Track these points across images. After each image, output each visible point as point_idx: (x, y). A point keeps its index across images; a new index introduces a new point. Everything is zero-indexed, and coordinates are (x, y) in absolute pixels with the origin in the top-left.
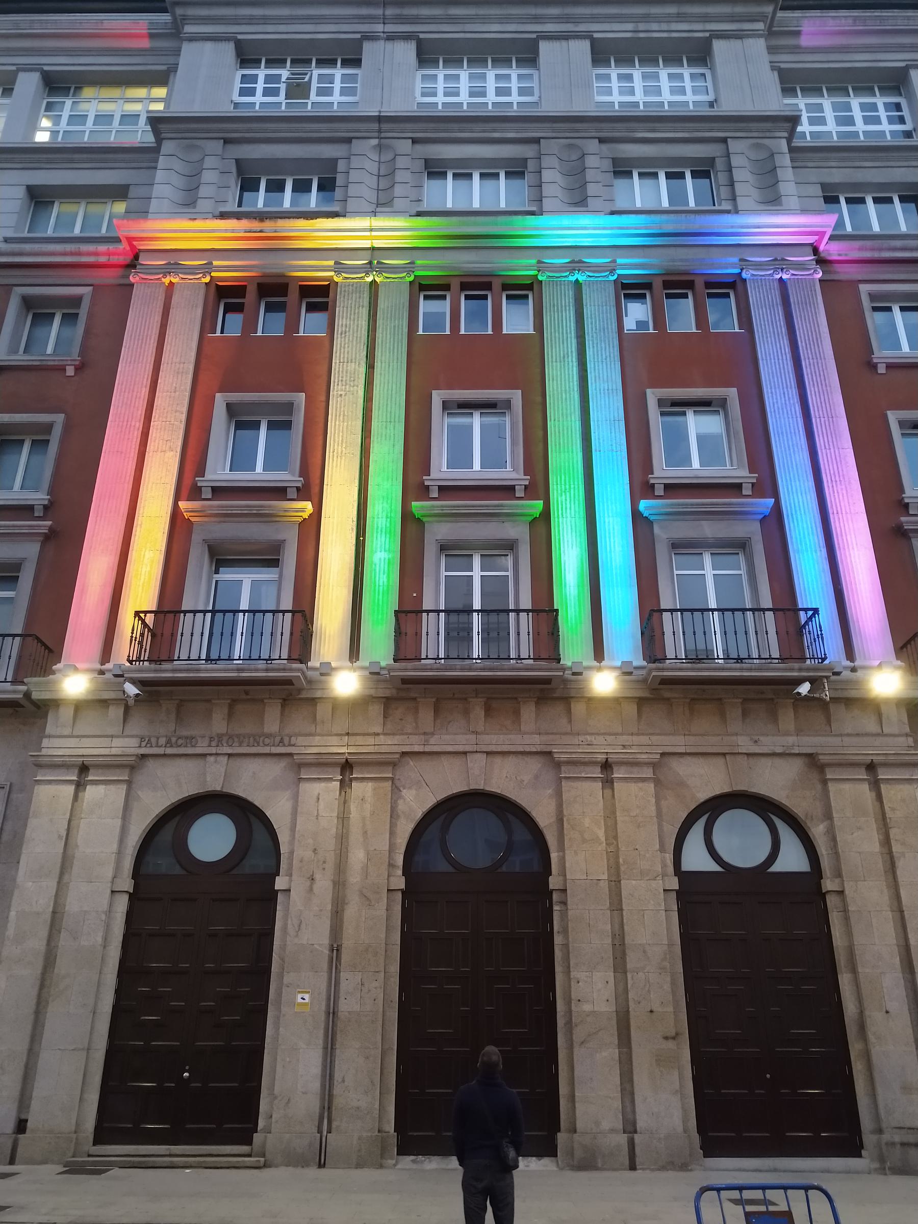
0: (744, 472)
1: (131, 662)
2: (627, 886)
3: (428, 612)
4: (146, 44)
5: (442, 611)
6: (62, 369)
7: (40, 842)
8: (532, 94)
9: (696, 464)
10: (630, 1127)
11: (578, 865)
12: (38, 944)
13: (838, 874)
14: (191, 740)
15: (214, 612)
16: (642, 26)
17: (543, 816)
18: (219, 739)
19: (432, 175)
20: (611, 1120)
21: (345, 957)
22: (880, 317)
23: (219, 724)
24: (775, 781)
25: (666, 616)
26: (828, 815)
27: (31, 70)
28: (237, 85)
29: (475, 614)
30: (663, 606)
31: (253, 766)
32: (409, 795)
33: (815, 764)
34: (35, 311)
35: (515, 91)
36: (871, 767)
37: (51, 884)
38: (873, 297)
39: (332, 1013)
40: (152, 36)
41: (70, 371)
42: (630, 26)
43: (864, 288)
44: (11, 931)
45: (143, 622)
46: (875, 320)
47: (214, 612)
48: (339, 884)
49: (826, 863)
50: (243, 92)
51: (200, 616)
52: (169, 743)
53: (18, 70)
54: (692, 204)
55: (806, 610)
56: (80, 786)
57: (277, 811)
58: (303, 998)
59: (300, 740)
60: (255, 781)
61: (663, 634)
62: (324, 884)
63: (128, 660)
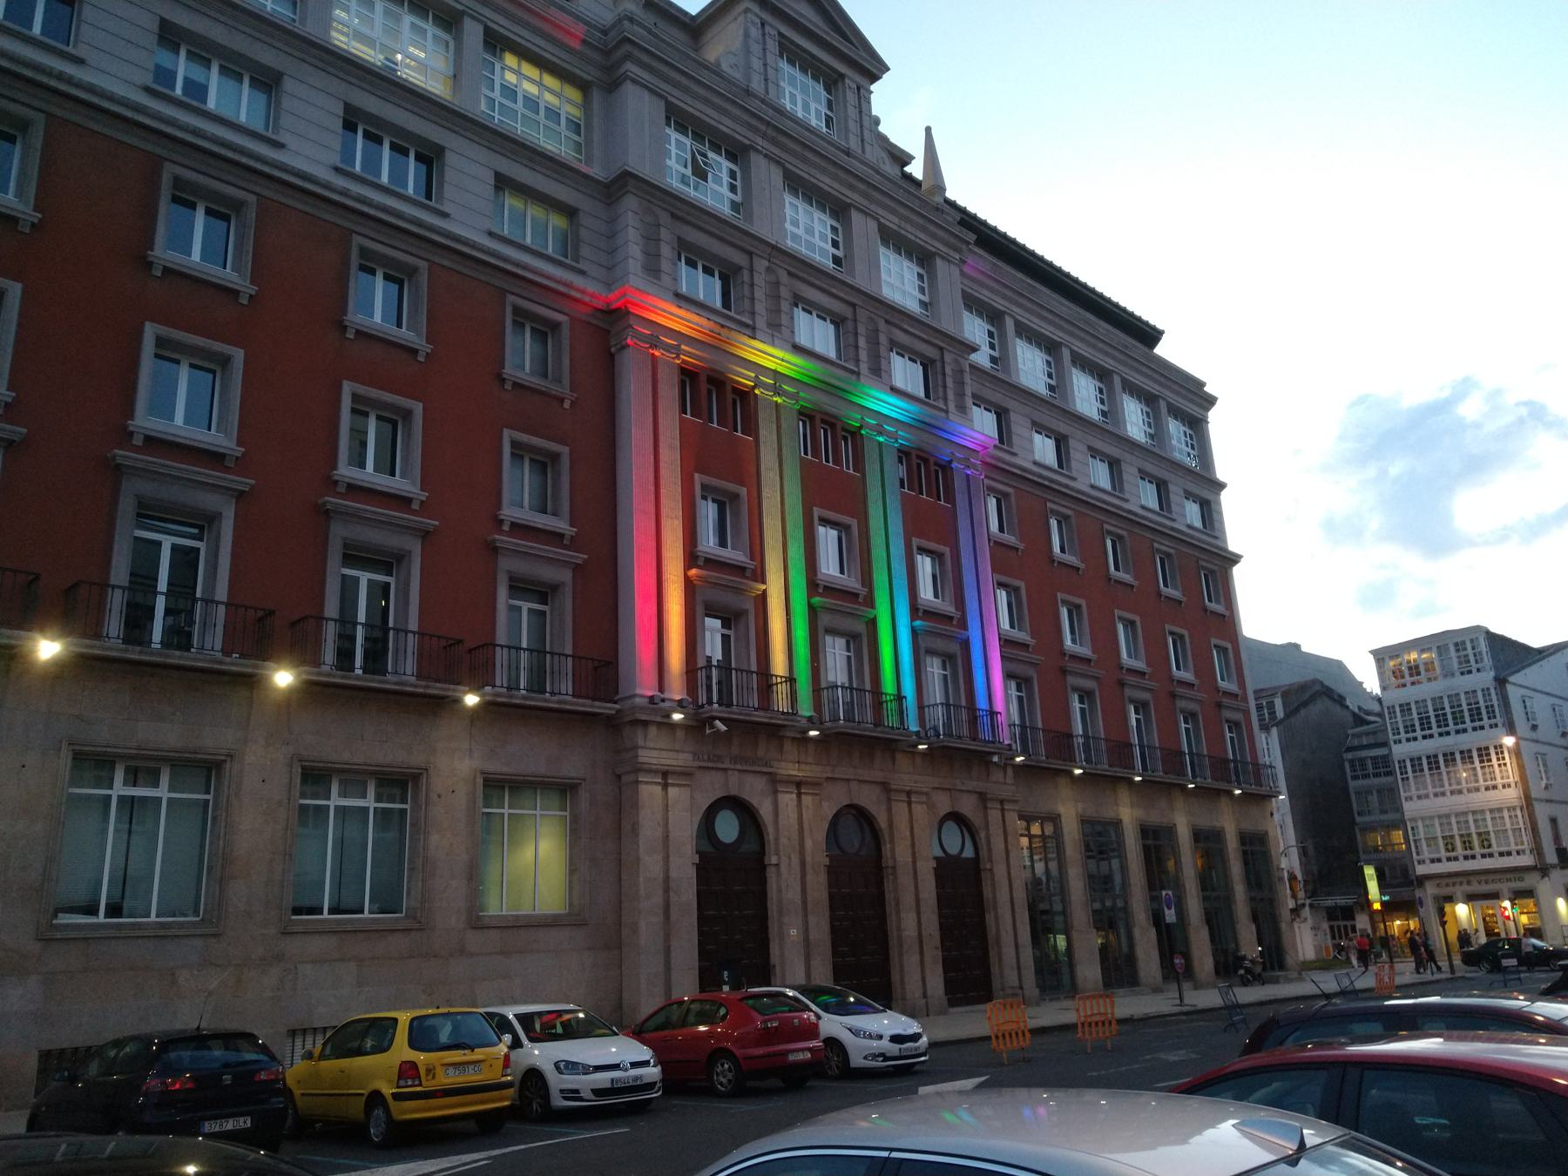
0: (233, 445)
2: (919, 864)
4: (577, 45)
6: (562, 400)
7: (649, 828)
9: (179, 418)
10: (925, 996)
11: (899, 852)
12: (658, 899)
13: (990, 860)
14: (720, 759)
16: (903, 224)
17: (882, 822)
18: (735, 760)
20: (918, 994)
21: (809, 906)
22: (363, 276)
23: (735, 750)
24: (968, 806)
26: (987, 828)
27: (479, 21)
29: (410, 636)
31: (750, 779)
32: (825, 804)
33: (983, 798)
34: (1493, 691)
36: (1002, 802)
37: (659, 857)
38: (177, 182)
39: (807, 940)
40: (584, 42)
41: (567, 405)
42: (896, 220)
43: (511, 298)
44: (642, 893)
46: (357, 280)
48: (803, 863)
49: (984, 853)
52: (709, 760)
56: (665, 786)
57: (765, 810)
58: (793, 932)
59: (775, 764)
60: (753, 790)
62: (795, 860)
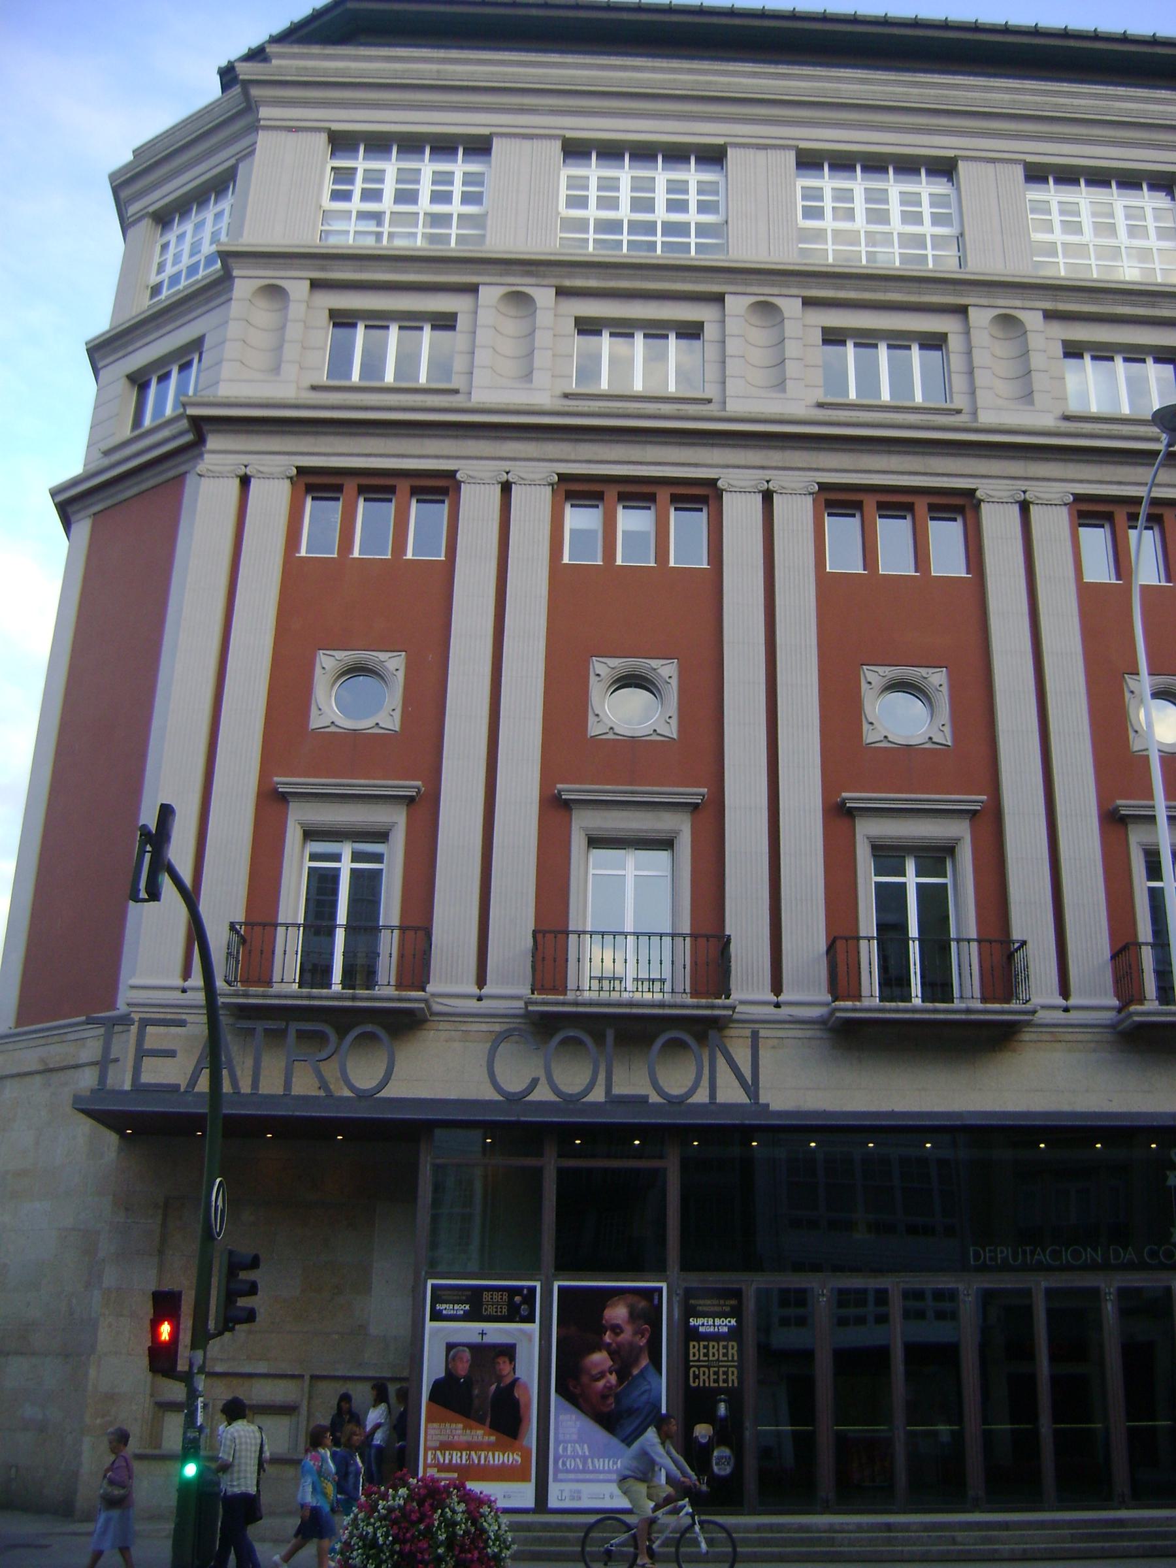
1: (229, 983)
3: (287, 926)
5: (973, 940)
8: (716, 212)
15: (673, 936)
19: (1068, 354)
25: (281, 930)
28: (328, 186)
30: (861, 935)
35: (693, 206)
45: (238, 932)
47: (673, 936)
50: (337, 196)
51: (655, 940)
53: (238, 161)
54: (355, 377)
55: (1018, 941)
61: (567, 960)
63: (226, 982)
